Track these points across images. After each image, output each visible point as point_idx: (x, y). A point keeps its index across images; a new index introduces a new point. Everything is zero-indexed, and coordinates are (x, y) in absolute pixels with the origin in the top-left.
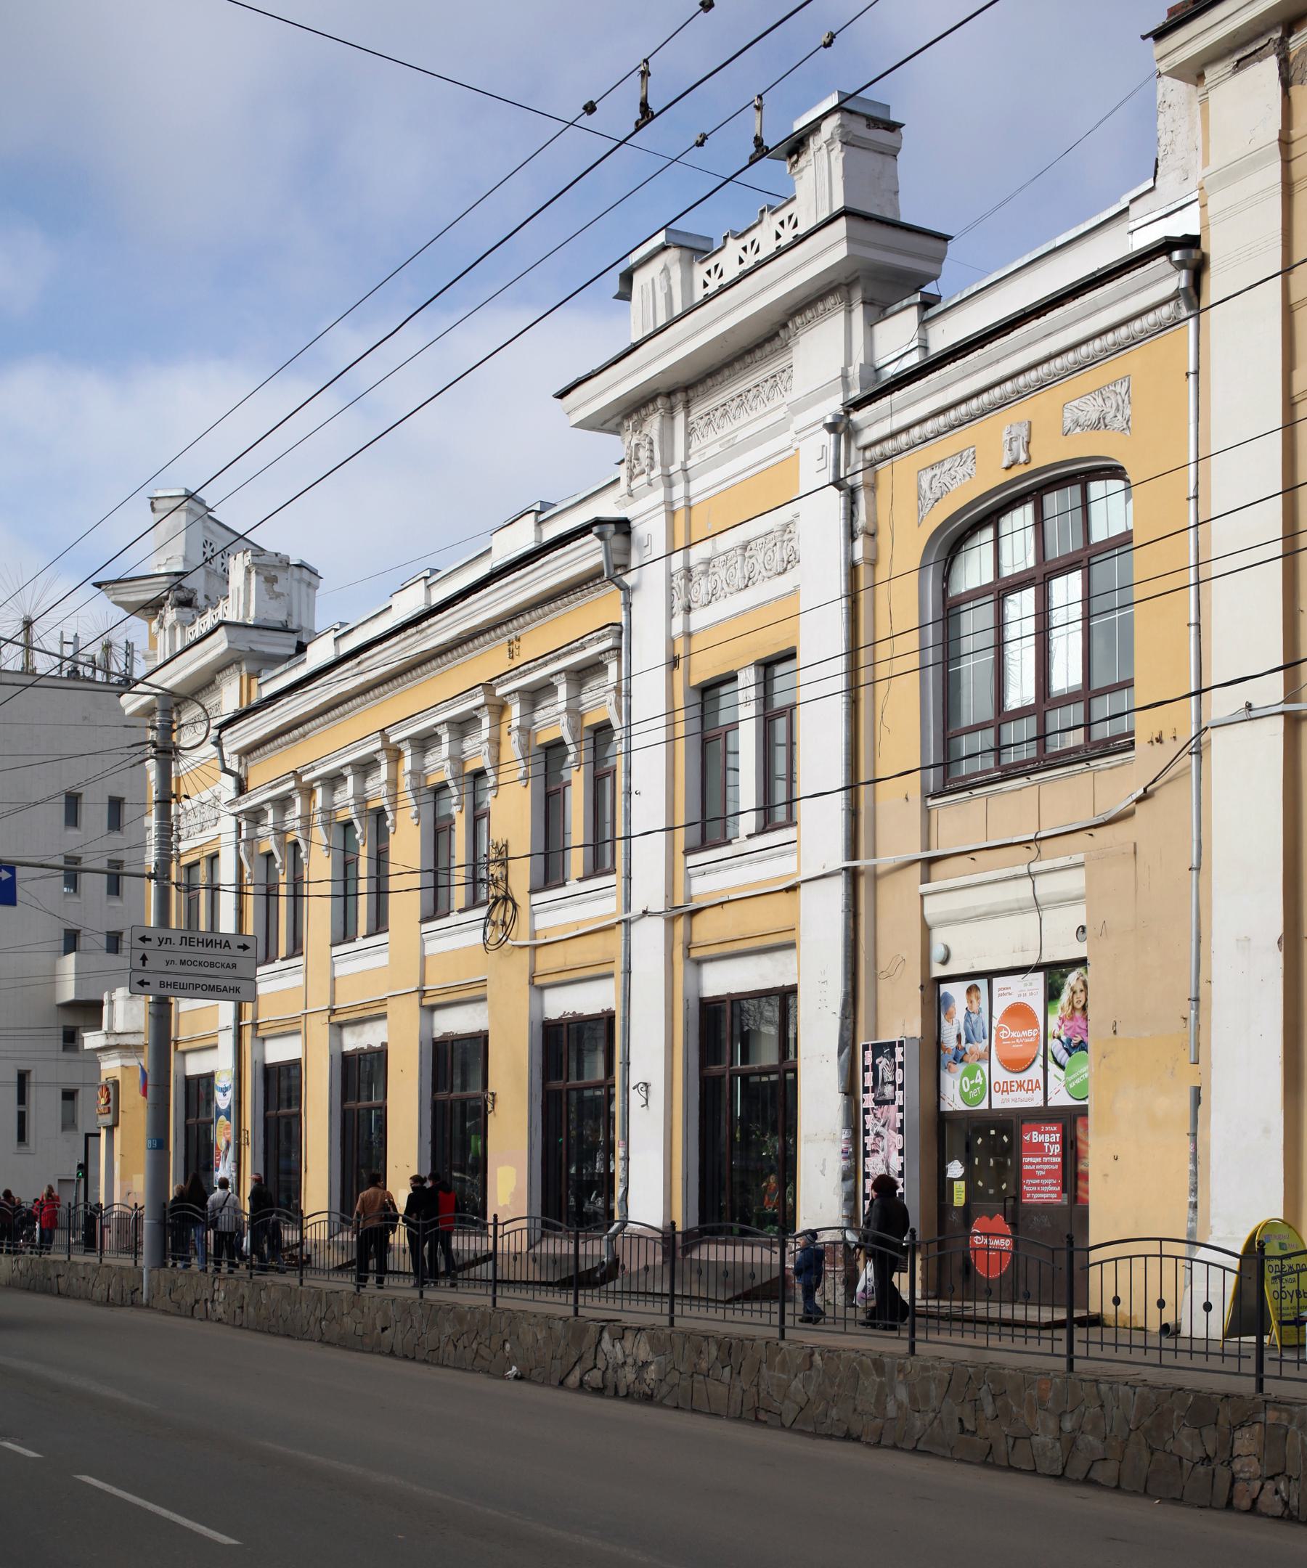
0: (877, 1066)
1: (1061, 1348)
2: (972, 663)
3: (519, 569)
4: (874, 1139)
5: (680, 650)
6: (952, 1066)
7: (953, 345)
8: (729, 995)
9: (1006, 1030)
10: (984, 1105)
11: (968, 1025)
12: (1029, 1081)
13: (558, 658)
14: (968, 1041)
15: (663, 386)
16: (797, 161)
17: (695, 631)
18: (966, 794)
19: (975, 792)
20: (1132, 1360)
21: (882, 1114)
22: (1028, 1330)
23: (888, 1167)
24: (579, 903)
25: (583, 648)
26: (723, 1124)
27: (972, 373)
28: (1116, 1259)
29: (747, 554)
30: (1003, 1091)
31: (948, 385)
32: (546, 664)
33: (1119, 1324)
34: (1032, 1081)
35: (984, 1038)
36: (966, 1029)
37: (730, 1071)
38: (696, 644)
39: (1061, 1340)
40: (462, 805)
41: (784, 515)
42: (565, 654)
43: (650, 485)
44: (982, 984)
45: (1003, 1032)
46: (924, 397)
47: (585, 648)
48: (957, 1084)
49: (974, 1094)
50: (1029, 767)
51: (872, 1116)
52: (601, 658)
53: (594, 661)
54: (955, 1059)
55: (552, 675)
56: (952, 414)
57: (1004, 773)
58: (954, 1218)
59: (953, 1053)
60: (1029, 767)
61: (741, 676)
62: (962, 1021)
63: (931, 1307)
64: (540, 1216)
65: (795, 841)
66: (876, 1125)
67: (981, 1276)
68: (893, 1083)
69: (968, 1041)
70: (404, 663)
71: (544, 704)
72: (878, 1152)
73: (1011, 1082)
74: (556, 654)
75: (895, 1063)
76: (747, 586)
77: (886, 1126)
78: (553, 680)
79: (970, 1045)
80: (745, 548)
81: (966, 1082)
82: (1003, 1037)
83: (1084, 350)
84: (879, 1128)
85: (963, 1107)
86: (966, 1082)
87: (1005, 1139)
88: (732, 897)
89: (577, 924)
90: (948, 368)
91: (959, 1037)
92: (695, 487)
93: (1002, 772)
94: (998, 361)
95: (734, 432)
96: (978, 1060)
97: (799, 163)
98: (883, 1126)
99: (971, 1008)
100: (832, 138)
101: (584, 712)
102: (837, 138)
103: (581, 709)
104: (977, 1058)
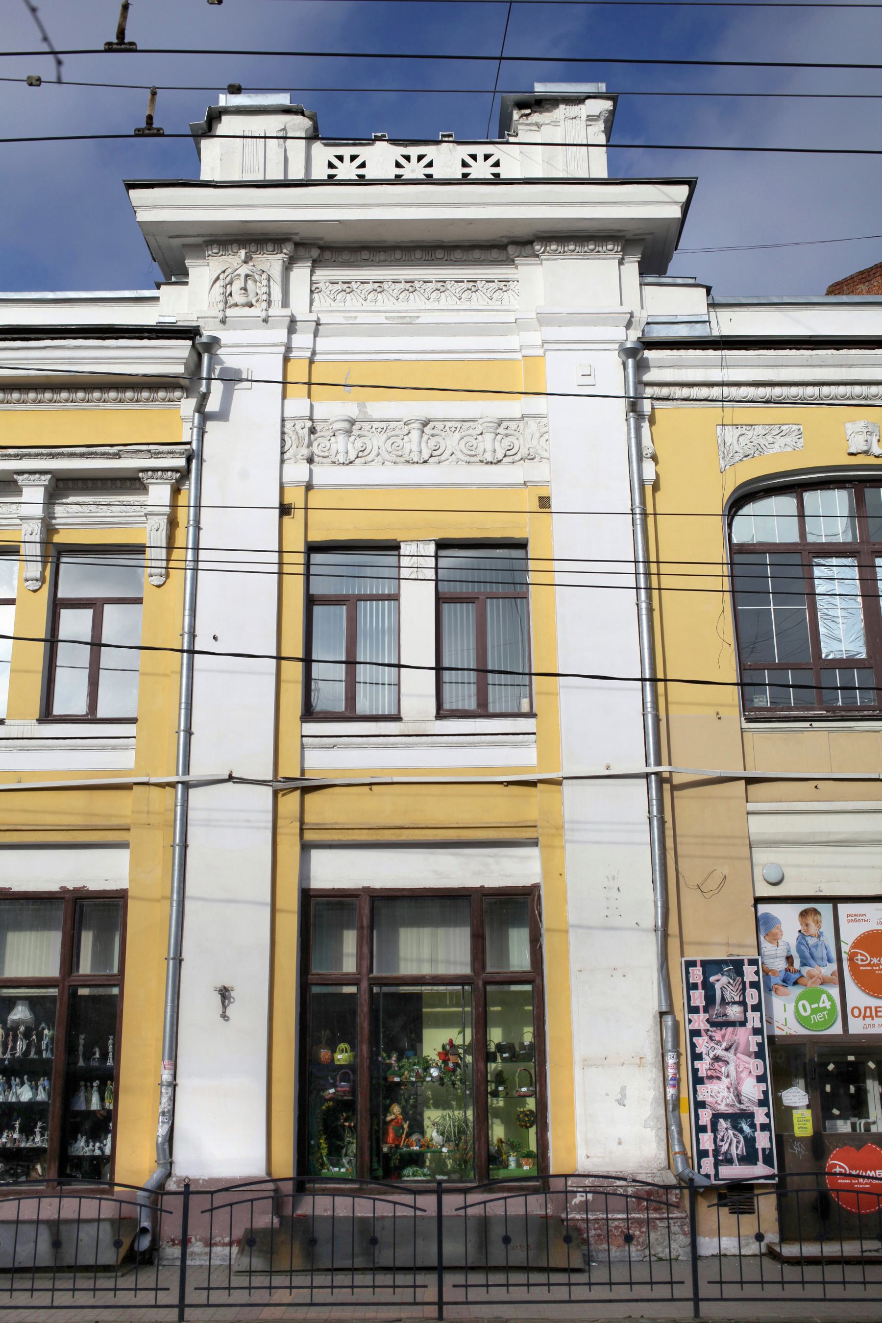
0: (712, 986)
1: (431, 1294)
2: (772, 607)
3: (52, 339)
4: (712, 1064)
5: (295, 497)
6: (781, 988)
7: (811, 336)
8: (367, 890)
9: (862, 955)
10: (837, 1029)
11: (803, 948)
12: (866, 1008)
13: (53, 456)
14: (803, 964)
15: (304, 233)
16: (527, 115)
17: (318, 485)
18: (807, 724)
19: (815, 724)
20: (530, 1299)
21: (723, 1037)
22: (531, 1276)
23: (738, 1095)
24: (22, 749)
25: (117, 455)
26: (670, 1039)
27: (779, 366)
28: (231, 1205)
29: (501, 430)
30: (865, 1017)
31: (782, 366)
32: (21, 457)
33: (672, 1257)
34: (870, 1008)
35: (829, 961)
36: (799, 950)
37: (370, 979)
38: (315, 499)
39: (682, 1283)
40: (43, 582)
41: (513, 407)
42: (82, 455)
43: (265, 321)
44: (825, 909)
45: (859, 957)
46: (745, 366)
47: (120, 457)
48: (791, 1007)
49: (818, 1017)
50: (866, 713)
51: (706, 1038)
52: (141, 475)
53: (134, 476)
54: (784, 981)
55: (21, 473)
56: (777, 391)
57: (829, 714)
58: (798, 1151)
59: (782, 975)
60: (866, 713)
61: (150, 553)
62: (793, 943)
63: (866, 1251)
64: (56, 1178)
65: (534, 734)
66: (713, 1049)
67: (850, 1212)
68: (743, 1003)
69: (803, 964)
70: (47, 376)
71: (72, 499)
72: (719, 1078)
73: (876, 1008)
74: (53, 451)
75: (744, 983)
76: (425, 462)
77: (732, 1051)
78: (20, 479)
79: (807, 968)
80: (425, 424)
81: (804, 1006)
82: (860, 963)
83: (825, 390)
84: (719, 1052)
85: (802, 1031)
86: (804, 1006)
87: (831, 1067)
88: (395, 780)
89: (18, 774)
90: (787, 352)
91: (789, 959)
92: (322, 344)
93: (827, 711)
94: (851, 366)
95: (420, 311)
96: (821, 984)
97: (530, 118)
98: (727, 1049)
99: (807, 931)
100: (599, 116)
101: (57, 527)
102: (602, 118)
103: (54, 522)
104: (819, 982)
